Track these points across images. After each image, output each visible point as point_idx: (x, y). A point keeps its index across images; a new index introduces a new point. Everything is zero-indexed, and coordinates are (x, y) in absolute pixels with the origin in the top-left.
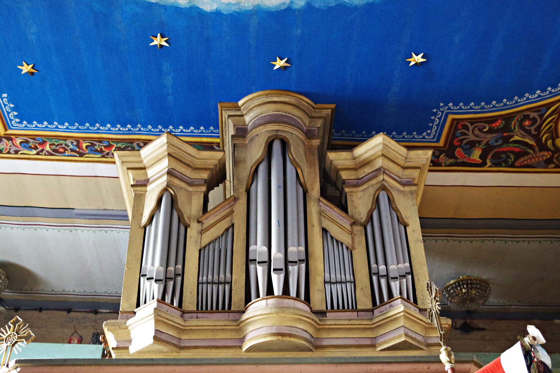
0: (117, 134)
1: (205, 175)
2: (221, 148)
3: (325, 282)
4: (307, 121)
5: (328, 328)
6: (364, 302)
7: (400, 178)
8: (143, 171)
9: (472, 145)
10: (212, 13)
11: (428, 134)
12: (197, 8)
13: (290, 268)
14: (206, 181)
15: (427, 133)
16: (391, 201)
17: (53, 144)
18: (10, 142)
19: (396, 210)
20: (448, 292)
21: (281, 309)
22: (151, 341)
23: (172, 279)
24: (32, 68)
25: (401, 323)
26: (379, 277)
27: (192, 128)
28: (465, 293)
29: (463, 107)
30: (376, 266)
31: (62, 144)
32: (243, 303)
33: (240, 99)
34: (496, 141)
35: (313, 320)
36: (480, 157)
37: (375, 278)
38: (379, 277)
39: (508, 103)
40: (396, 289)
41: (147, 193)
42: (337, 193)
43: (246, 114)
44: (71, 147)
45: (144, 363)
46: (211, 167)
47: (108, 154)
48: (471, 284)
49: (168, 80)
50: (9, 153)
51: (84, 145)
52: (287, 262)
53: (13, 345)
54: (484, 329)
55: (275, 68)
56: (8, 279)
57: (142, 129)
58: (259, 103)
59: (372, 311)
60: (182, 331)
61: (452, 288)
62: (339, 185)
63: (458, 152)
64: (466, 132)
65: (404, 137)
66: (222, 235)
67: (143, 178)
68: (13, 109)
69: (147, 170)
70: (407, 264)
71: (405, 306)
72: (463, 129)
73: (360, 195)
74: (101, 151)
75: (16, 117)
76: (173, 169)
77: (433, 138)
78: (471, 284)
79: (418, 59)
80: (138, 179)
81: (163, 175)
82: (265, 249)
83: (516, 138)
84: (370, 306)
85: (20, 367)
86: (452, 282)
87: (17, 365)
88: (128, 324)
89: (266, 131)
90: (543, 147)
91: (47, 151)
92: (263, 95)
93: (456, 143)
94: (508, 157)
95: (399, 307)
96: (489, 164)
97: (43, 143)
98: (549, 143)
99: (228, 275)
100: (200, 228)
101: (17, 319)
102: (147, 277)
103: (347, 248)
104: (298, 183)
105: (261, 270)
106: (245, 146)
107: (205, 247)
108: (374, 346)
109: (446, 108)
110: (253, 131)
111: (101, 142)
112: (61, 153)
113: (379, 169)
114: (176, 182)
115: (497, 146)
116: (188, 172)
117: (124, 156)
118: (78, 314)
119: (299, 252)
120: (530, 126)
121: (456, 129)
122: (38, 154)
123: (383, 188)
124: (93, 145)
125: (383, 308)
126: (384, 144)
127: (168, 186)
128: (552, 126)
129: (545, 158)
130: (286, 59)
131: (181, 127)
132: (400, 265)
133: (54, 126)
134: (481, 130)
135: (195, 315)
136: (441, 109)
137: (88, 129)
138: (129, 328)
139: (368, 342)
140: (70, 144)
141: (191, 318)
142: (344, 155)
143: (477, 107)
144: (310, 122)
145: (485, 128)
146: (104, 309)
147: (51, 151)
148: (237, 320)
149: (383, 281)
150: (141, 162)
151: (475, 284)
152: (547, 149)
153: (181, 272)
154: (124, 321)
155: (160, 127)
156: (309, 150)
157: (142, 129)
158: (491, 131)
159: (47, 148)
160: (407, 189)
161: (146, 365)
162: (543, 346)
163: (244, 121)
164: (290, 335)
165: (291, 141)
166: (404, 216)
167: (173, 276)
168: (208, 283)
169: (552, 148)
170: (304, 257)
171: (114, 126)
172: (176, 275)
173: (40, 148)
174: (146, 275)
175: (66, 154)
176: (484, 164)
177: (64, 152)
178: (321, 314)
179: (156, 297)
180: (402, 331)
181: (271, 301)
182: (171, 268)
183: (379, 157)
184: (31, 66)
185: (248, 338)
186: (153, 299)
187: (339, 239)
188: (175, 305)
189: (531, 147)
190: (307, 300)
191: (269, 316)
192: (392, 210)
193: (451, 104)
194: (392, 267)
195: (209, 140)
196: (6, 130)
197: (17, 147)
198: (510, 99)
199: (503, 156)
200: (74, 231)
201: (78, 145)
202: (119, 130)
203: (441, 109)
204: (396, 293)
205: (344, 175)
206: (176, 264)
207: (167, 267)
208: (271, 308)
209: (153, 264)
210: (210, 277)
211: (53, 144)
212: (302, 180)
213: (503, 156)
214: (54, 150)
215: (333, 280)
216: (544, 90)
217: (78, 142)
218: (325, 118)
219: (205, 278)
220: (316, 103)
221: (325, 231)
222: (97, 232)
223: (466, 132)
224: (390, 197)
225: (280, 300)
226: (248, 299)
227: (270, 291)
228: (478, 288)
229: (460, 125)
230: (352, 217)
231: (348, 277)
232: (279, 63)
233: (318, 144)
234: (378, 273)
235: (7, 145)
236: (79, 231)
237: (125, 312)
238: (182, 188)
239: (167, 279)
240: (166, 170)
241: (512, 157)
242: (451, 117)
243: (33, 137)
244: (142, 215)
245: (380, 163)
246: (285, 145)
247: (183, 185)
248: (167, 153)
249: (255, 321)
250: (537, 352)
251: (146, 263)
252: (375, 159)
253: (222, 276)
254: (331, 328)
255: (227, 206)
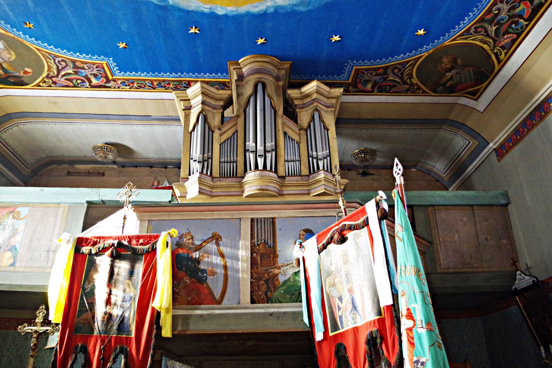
0: (173, 78)
1: (222, 103)
2: (230, 88)
3: (285, 161)
4: (276, 71)
5: (286, 186)
6: (305, 171)
7: (326, 103)
8: (189, 101)
9: (367, 82)
10: (223, 15)
11: (343, 76)
12: (214, 13)
13: (267, 154)
14: (222, 106)
15: (342, 76)
16: (320, 117)
17: (139, 83)
18: (115, 82)
19: (323, 122)
20: (354, 156)
21: (262, 177)
22: (198, 193)
23: (206, 160)
24: (125, 45)
25: (323, 183)
26: (313, 158)
27: (214, 74)
28: (363, 157)
29: (361, 63)
30: (311, 152)
31: (143, 83)
32: (243, 173)
33: (239, 59)
34: (380, 80)
35: (278, 182)
36: (371, 88)
37: (311, 159)
38: (313, 158)
39: (386, 61)
40: (321, 165)
41: (191, 114)
42: (292, 110)
43: (243, 67)
44: (148, 84)
45: (194, 205)
46: (225, 99)
47: (168, 88)
48: (366, 152)
49: (200, 50)
50: (115, 88)
51: (155, 84)
52: (265, 151)
53: (129, 197)
54: (374, 174)
55: (258, 43)
56: (118, 152)
57: (186, 75)
58: (250, 62)
59: (309, 176)
60: (212, 187)
61: (357, 154)
62: (294, 107)
63: (359, 85)
64: (363, 75)
65: (329, 78)
66: (232, 136)
67: (188, 105)
68: (116, 66)
69: (191, 101)
70: (328, 151)
71: (325, 174)
72: (361, 74)
73: (304, 113)
74: (165, 87)
75: (117, 70)
76: (204, 100)
77: (346, 78)
78: (366, 152)
79: (337, 38)
80: (186, 105)
81: (199, 104)
82: (254, 144)
83: (390, 78)
84: (308, 173)
85: (134, 207)
86: (357, 151)
87: (132, 207)
88: (185, 185)
89: (254, 78)
90: (405, 83)
91: (136, 87)
92: (252, 57)
93: (358, 80)
94: (386, 88)
95: (322, 175)
96: (376, 91)
97: (133, 83)
98: (408, 81)
99: (235, 158)
100: (220, 133)
101: (130, 183)
102: (194, 160)
103: (297, 143)
104: (272, 107)
105: (252, 156)
106: (243, 86)
107: (223, 143)
108: (309, 194)
109: (352, 63)
110: (247, 78)
111: (164, 82)
112: (143, 87)
113: (315, 99)
114: (206, 108)
115: (380, 83)
116: (212, 102)
117: (178, 93)
118: (156, 169)
119: (272, 145)
120: (398, 72)
121: (358, 74)
122: (130, 88)
123: (317, 110)
124: (160, 83)
125: (314, 175)
126: (318, 86)
127: (202, 110)
128: (409, 72)
129: (406, 88)
130: (264, 39)
131: (208, 74)
132: (323, 152)
133: (139, 74)
134: (371, 74)
135: (218, 179)
136: (350, 64)
137: (157, 75)
138: (186, 187)
139: (306, 192)
140: (147, 83)
141: (217, 181)
142: (296, 91)
143: (369, 63)
144: (278, 71)
145: (373, 73)
146: (170, 166)
147: (137, 87)
148: (240, 182)
149: (315, 161)
150: (187, 96)
151: (368, 152)
152: (407, 84)
153: (211, 157)
154: (183, 183)
155: (196, 74)
156: (277, 88)
157: (186, 75)
158: (377, 75)
159: (135, 85)
160: (329, 109)
161: (195, 206)
162: (385, 200)
163: (242, 72)
164: (267, 190)
165: (267, 84)
166: (327, 125)
167: (207, 159)
168: (225, 162)
169: (409, 83)
170: (274, 148)
171: (171, 73)
172: (209, 158)
173: (131, 86)
174: (193, 159)
175: (146, 88)
176: (373, 91)
177: (145, 87)
178: (283, 177)
179: (199, 171)
180: (323, 187)
181: (257, 172)
182: (206, 155)
183: (315, 93)
184: (125, 44)
185: (245, 191)
186: (197, 172)
187: (292, 138)
188: (208, 174)
189: (398, 83)
190: (276, 171)
191: (256, 180)
192: (321, 122)
193: (355, 61)
194: (320, 153)
195: (224, 80)
196: (113, 76)
197: (119, 85)
198: (387, 59)
199: (383, 87)
200: (152, 127)
201: (152, 84)
202: (174, 76)
203: (350, 64)
204: (321, 168)
205: (296, 102)
206: (208, 153)
207: (204, 154)
208: (257, 176)
209: (196, 153)
210: (226, 159)
211: (139, 83)
212: (273, 105)
213: (383, 87)
214: (139, 86)
215: (289, 160)
216: (405, 54)
217: (152, 82)
218: (286, 69)
219: (223, 159)
220: (281, 61)
221: (285, 133)
222: (165, 127)
223: (363, 75)
224: (320, 115)
225: (262, 172)
226: (246, 171)
227: (257, 167)
228: (370, 155)
229: (360, 72)
230: (300, 126)
231: (297, 158)
232: (260, 41)
233: (282, 84)
234: (312, 156)
235: (113, 84)
236: (155, 127)
237: (183, 178)
238: (209, 111)
239: (204, 161)
240: (201, 101)
241: (388, 88)
242: (355, 68)
243: (128, 80)
244: (189, 126)
245: (315, 96)
246: (264, 86)
247: (210, 109)
248: (201, 92)
249: (249, 183)
250: (382, 203)
251: (193, 152)
252: (312, 94)
253: (232, 158)
254: (288, 186)
255: (234, 121)
